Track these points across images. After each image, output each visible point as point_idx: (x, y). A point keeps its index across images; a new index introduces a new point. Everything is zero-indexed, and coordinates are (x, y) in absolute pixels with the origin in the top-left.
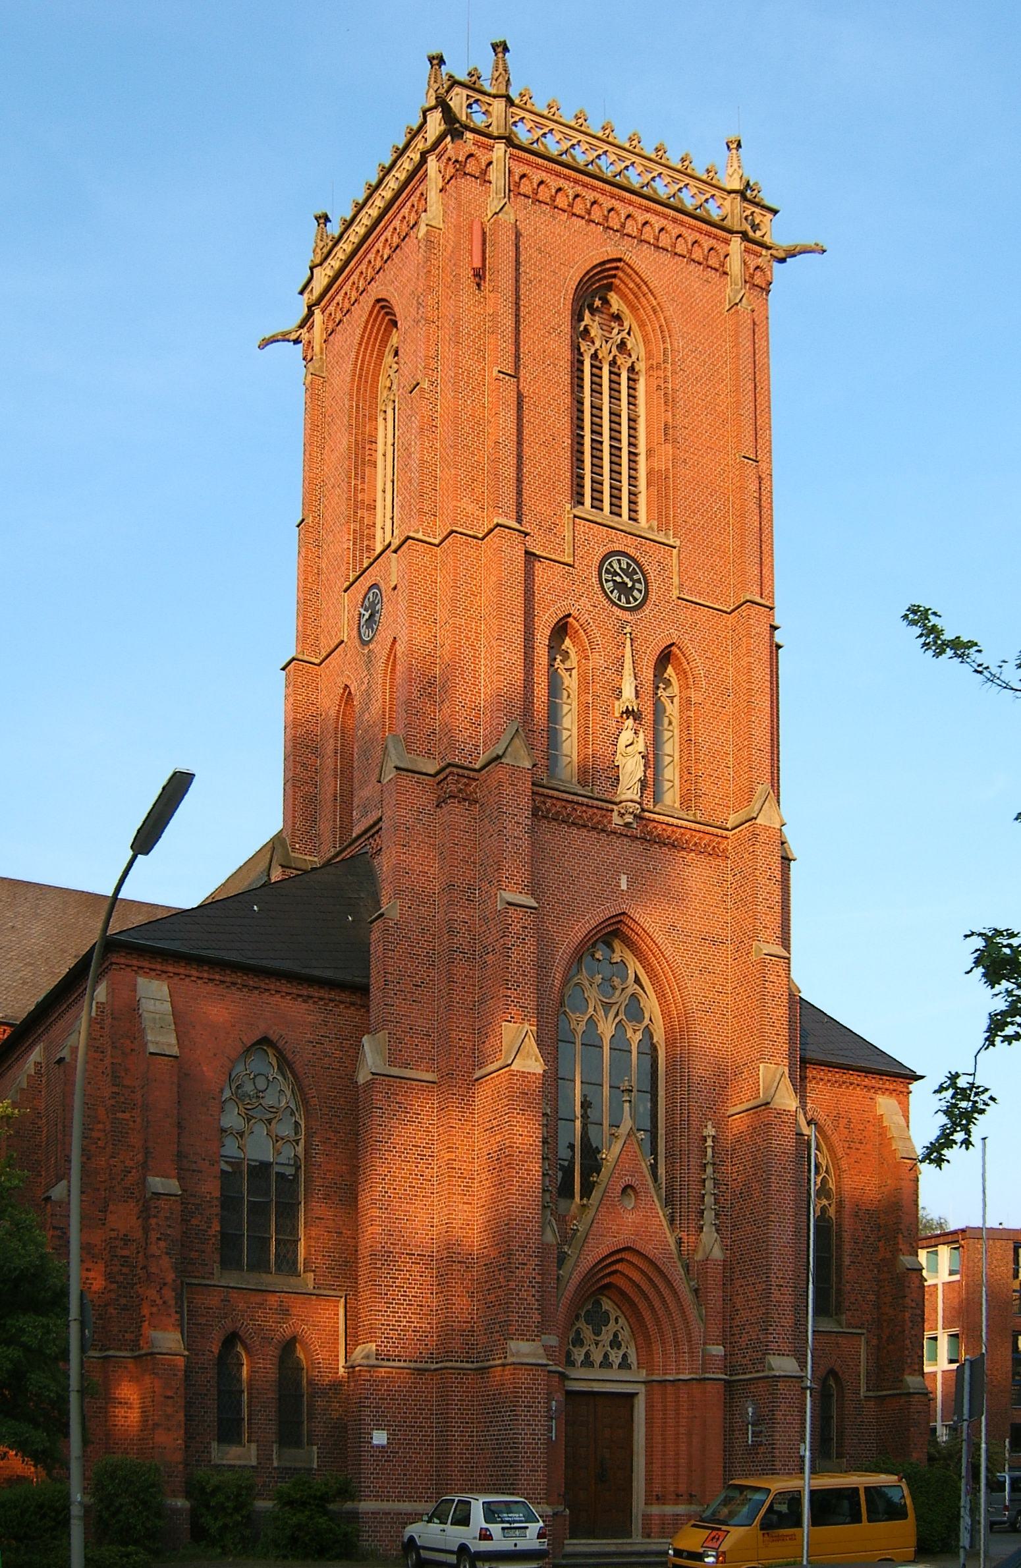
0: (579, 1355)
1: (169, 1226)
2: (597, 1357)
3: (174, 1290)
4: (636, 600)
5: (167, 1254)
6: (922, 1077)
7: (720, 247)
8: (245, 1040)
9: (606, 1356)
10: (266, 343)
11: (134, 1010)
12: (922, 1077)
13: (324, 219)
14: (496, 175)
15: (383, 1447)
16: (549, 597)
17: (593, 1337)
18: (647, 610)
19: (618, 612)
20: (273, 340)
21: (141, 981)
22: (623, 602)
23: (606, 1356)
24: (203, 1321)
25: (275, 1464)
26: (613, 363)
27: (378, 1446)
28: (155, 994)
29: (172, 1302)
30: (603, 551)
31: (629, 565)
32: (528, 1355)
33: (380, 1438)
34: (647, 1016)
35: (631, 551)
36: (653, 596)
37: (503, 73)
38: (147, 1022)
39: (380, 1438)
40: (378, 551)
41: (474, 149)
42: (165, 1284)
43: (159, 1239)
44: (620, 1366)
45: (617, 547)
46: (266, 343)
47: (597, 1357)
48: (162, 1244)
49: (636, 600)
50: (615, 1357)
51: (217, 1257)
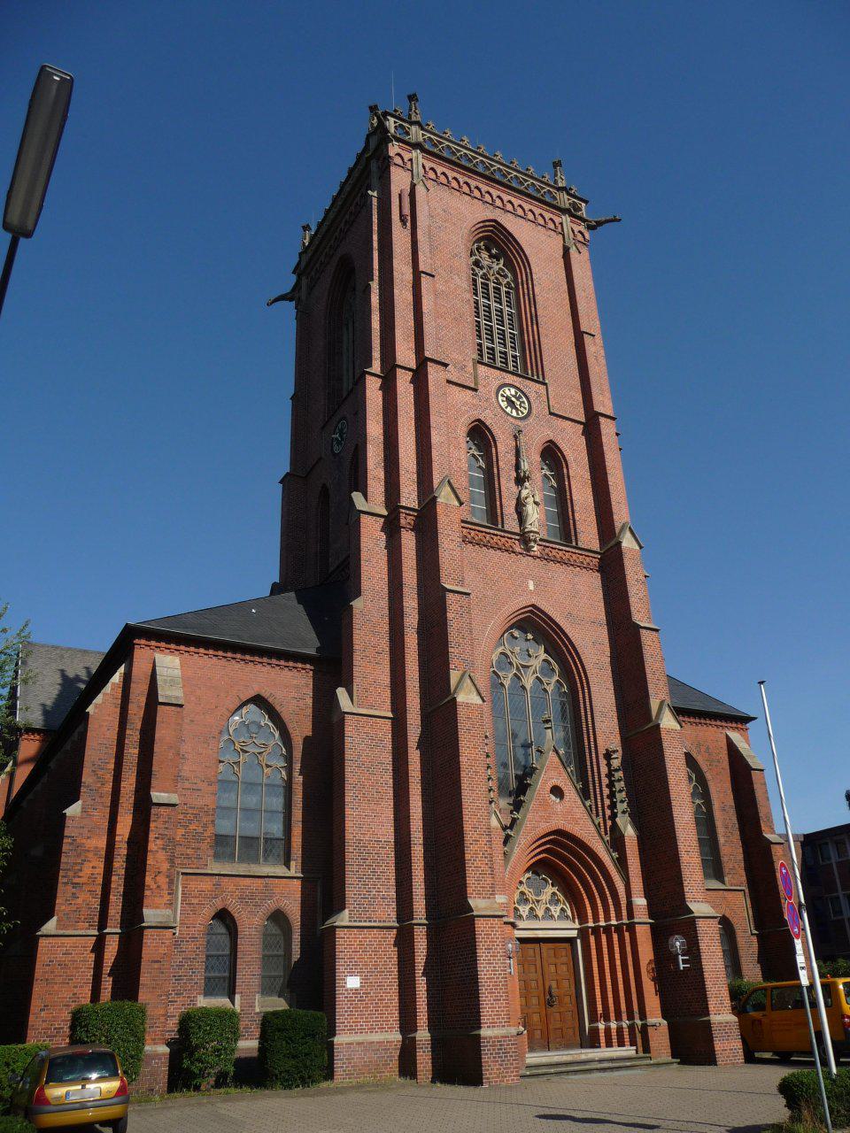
0: (524, 910)
1: (167, 828)
2: (540, 913)
3: (168, 876)
4: (523, 413)
5: (163, 849)
6: (754, 719)
8: (241, 696)
9: (548, 909)
12: (754, 719)
13: (306, 228)
15: (356, 990)
16: (463, 408)
17: (534, 897)
18: (531, 420)
19: (512, 420)
20: (277, 300)
21: (159, 657)
22: (514, 414)
23: (548, 909)
24: (195, 901)
25: (257, 1010)
27: (351, 990)
28: (169, 664)
29: (165, 887)
30: (499, 383)
31: (516, 393)
32: (486, 909)
33: (353, 982)
34: (473, 424)
36: (534, 411)
39: (353, 982)
40: (344, 396)
41: (400, 151)
42: (159, 873)
43: (156, 838)
44: (528, 918)
45: (507, 381)
47: (540, 913)
48: (158, 842)
49: (523, 413)
50: (556, 911)
51: (211, 852)
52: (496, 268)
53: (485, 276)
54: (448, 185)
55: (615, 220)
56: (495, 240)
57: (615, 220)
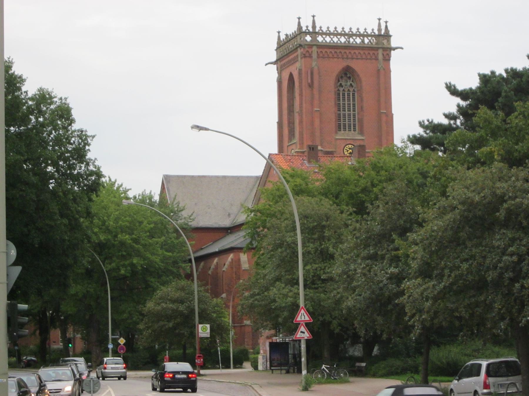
7: (376, 53)
10: (266, 64)
11: (239, 260)
14: (315, 55)
26: (349, 90)
28: (244, 257)
35: (352, 143)
37: (314, 27)
38: (242, 263)
45: (348, 143)
46: (266, 64)
52: (349, 84)
53: (344, 90)
54: (329, 57)
55: (402, 48)
56: (347, 73)
57: (402, 48)
